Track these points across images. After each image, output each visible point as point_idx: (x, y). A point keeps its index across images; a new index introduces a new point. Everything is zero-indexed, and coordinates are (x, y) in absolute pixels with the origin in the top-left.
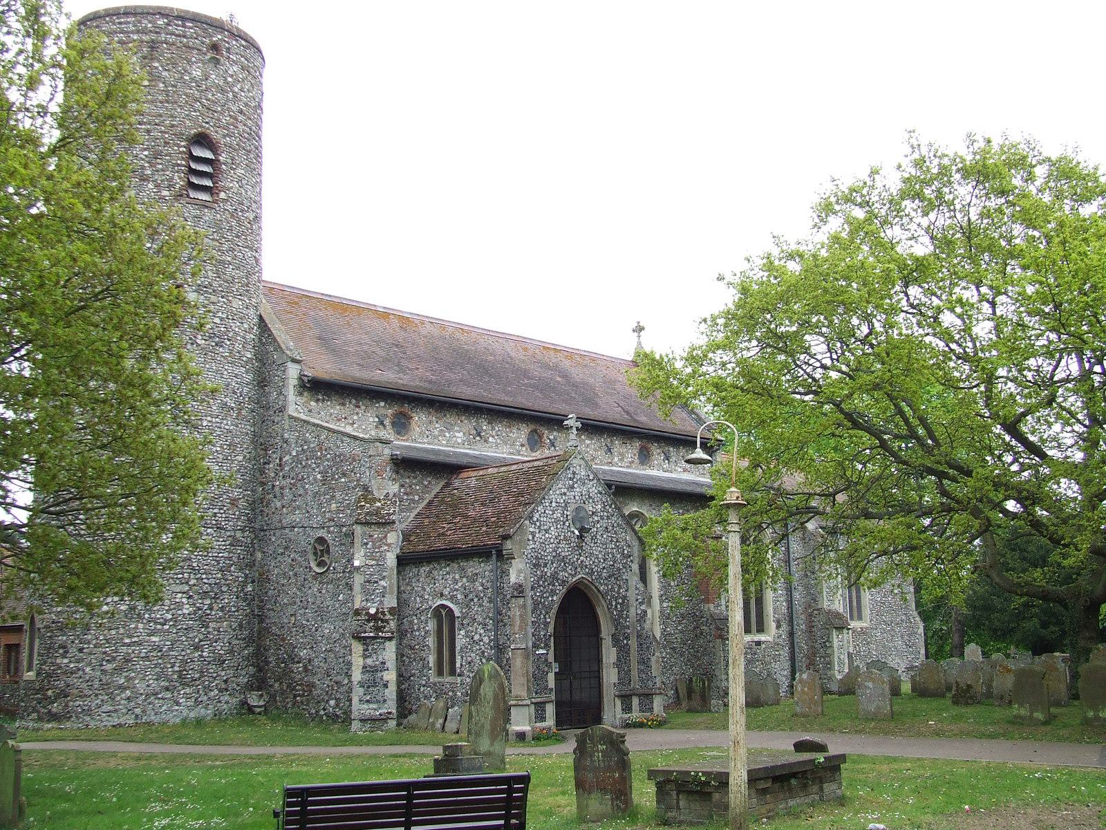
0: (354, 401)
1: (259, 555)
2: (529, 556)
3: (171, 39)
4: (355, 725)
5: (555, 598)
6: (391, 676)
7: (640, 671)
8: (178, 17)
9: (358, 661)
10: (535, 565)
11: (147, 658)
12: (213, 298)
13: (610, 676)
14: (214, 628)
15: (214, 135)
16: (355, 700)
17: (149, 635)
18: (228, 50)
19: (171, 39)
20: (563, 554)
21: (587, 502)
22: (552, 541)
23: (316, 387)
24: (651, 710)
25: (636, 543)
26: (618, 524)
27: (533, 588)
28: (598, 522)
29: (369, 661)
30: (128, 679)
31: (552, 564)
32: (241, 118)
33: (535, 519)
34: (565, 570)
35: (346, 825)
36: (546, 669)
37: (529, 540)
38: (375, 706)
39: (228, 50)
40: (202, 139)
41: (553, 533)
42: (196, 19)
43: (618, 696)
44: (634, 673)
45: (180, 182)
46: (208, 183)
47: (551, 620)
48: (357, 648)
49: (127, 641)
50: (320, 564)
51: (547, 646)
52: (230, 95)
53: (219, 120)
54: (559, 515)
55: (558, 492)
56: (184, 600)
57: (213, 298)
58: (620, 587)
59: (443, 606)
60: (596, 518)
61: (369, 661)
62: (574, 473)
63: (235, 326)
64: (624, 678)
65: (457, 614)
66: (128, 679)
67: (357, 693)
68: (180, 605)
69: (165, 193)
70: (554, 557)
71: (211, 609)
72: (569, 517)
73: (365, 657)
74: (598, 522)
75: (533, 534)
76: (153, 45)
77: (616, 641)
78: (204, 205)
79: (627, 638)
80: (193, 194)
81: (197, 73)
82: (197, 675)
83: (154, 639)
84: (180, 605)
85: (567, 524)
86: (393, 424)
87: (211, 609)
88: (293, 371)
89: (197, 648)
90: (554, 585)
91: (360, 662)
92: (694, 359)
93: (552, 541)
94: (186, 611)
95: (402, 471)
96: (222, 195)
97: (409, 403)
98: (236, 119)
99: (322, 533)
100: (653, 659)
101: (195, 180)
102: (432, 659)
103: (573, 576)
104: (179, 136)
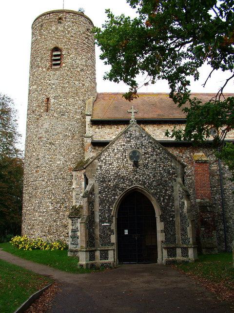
0: (116, 126)
2: (97, 177)
3: (46, 21)
5: (116, 197)
7: (182, 235)
10: (102, 182)
11: (38, 225)
12: (60, 100)
13: (160, 237)
14: (62, 215)
17: (39, 217)
19: (46, 21)
20: (122, 175)
21: (140, 148)
22: (114, 169)
23: (94, 123)
24: (187, 256)
25: (179, 167)
26: (165, 158)
27: (100, 193)
28: (149, 157)
29: (73, 227)
30: (34, 232)
31: (114, 180)
32: (72, 38)
33: (102, 159)
34: (124, 183)
35: (24, 302)
36: (109, 233)
37: (97, 169)
38: (75, 246)
41: (115, 165)
42: (53, 12)
43: (165, 248)
44: (178, 236)
47: (114, 209)
51: (110, 221)
53: (62, 41)
54: (119, 156)
55: (119, 145)
56: (50, 205)
57: (60, 100)
58: (166, 190)
60: (147, 156)
61: (73, 227)
62: (131, 134)
64: (167, 240)
66: (34, 232)
68: (48, 207)
69: (44, 69)
70: (116, 177)
71: (61, 208)
72: (127, 157)
74: (149, 157)
75: (101, 167)
76: (42, 26)
77: (163, 219)
78: (57, 70)
79: (173, 217)
80: (53, 67)
82: (55, 231)
83: (40, 218)
84: (48, 207)
85: (125, 160)
87: (61, 208)
89: (55, 221)
90: (116, 191)
93: (114, 169)
94: (50, 209)
95: (97, 148)
96: (64, 65)
97: (143, 124)
98: (70, 39)
100: (188, 228)
103: (130, 186)
104: (48, 50)
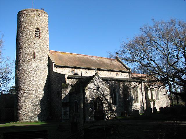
1: (50, 94)
4: (63, 121)
6: (68, 113)
8: (116, 81)
9: (63, 111)
15: (39, 28)
16: (63, 117)
18: (41, 14)
29: (65, 111)
39: (41, 14)
40: (37, 29)
45: (34, 35)
46: (38, 35)
48: (63, 108)
49: (28, 108)
50: (58, 95)
52: (42, 21)
57: (40, 54)
59: (76, 101)
61: (65, 111)
63: (44, 58)
65: (78, 102)
67: (63, 116)
73: (64, 110)
80: (36, 37)
81: (36, 19)
86: (71, 72)
88: (53, 64)
91: (63, 111)
92: (121, 93)
99: (58, 90)
101: (36, 35)
102: (75, 110)
